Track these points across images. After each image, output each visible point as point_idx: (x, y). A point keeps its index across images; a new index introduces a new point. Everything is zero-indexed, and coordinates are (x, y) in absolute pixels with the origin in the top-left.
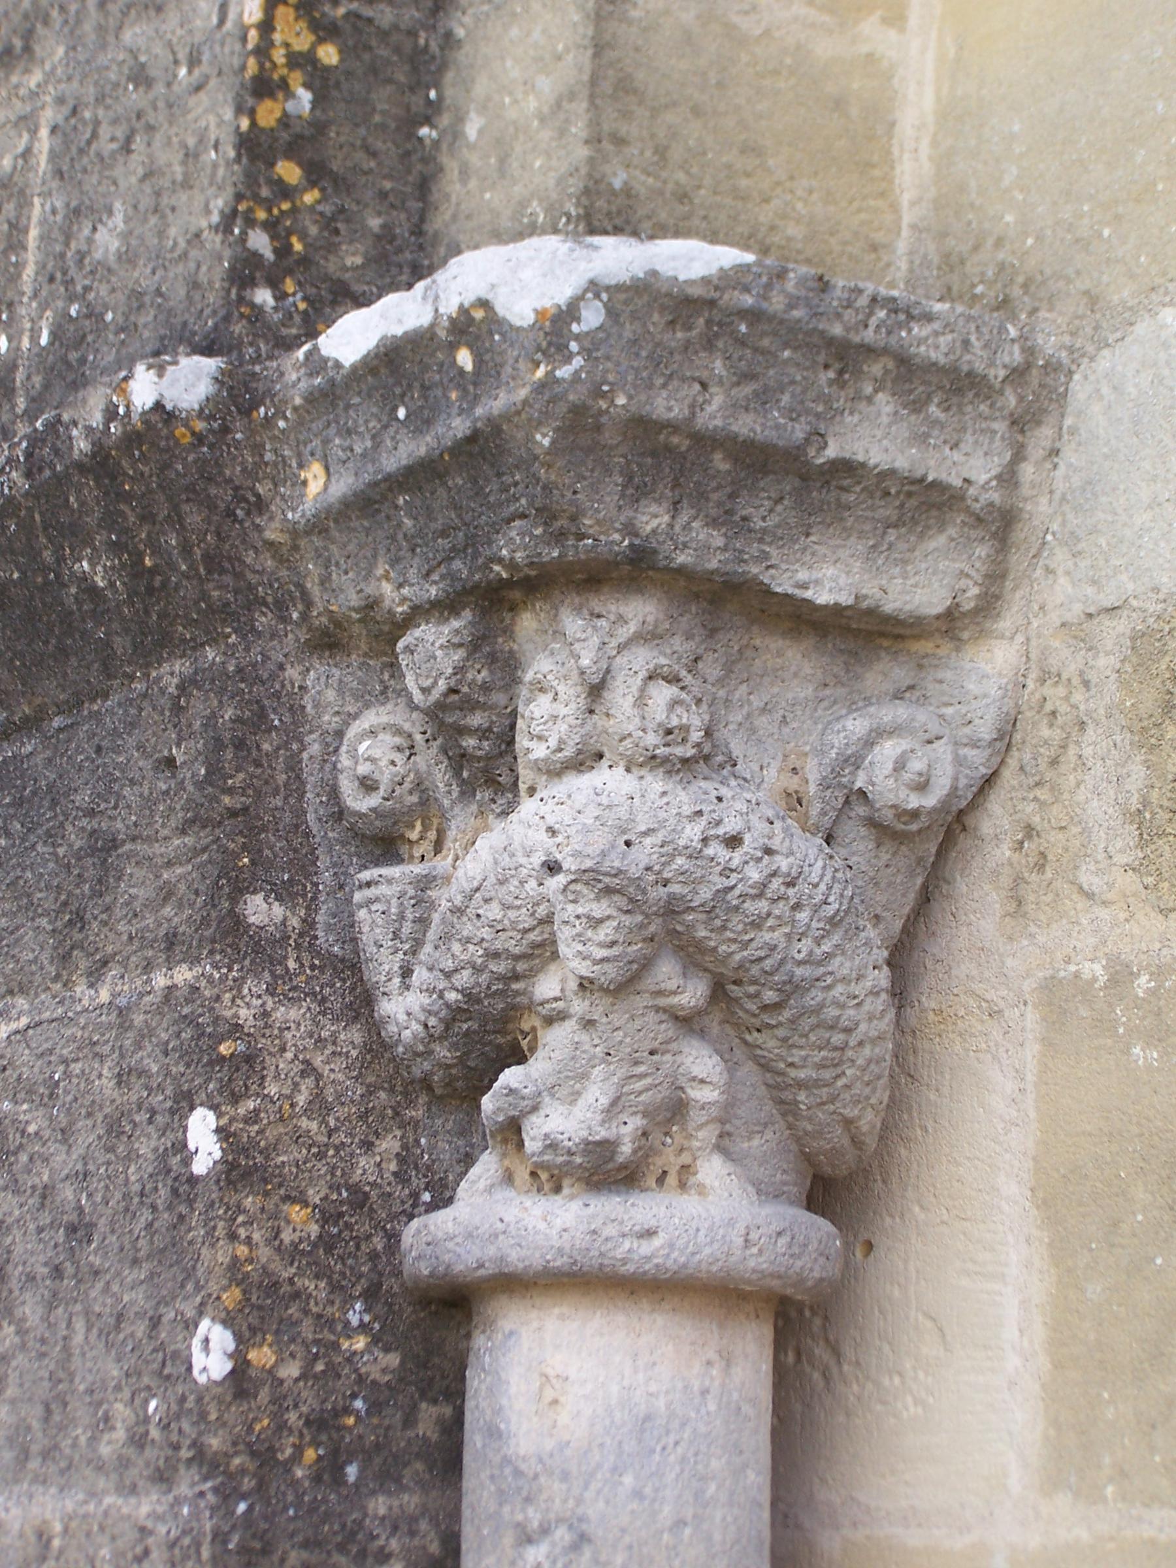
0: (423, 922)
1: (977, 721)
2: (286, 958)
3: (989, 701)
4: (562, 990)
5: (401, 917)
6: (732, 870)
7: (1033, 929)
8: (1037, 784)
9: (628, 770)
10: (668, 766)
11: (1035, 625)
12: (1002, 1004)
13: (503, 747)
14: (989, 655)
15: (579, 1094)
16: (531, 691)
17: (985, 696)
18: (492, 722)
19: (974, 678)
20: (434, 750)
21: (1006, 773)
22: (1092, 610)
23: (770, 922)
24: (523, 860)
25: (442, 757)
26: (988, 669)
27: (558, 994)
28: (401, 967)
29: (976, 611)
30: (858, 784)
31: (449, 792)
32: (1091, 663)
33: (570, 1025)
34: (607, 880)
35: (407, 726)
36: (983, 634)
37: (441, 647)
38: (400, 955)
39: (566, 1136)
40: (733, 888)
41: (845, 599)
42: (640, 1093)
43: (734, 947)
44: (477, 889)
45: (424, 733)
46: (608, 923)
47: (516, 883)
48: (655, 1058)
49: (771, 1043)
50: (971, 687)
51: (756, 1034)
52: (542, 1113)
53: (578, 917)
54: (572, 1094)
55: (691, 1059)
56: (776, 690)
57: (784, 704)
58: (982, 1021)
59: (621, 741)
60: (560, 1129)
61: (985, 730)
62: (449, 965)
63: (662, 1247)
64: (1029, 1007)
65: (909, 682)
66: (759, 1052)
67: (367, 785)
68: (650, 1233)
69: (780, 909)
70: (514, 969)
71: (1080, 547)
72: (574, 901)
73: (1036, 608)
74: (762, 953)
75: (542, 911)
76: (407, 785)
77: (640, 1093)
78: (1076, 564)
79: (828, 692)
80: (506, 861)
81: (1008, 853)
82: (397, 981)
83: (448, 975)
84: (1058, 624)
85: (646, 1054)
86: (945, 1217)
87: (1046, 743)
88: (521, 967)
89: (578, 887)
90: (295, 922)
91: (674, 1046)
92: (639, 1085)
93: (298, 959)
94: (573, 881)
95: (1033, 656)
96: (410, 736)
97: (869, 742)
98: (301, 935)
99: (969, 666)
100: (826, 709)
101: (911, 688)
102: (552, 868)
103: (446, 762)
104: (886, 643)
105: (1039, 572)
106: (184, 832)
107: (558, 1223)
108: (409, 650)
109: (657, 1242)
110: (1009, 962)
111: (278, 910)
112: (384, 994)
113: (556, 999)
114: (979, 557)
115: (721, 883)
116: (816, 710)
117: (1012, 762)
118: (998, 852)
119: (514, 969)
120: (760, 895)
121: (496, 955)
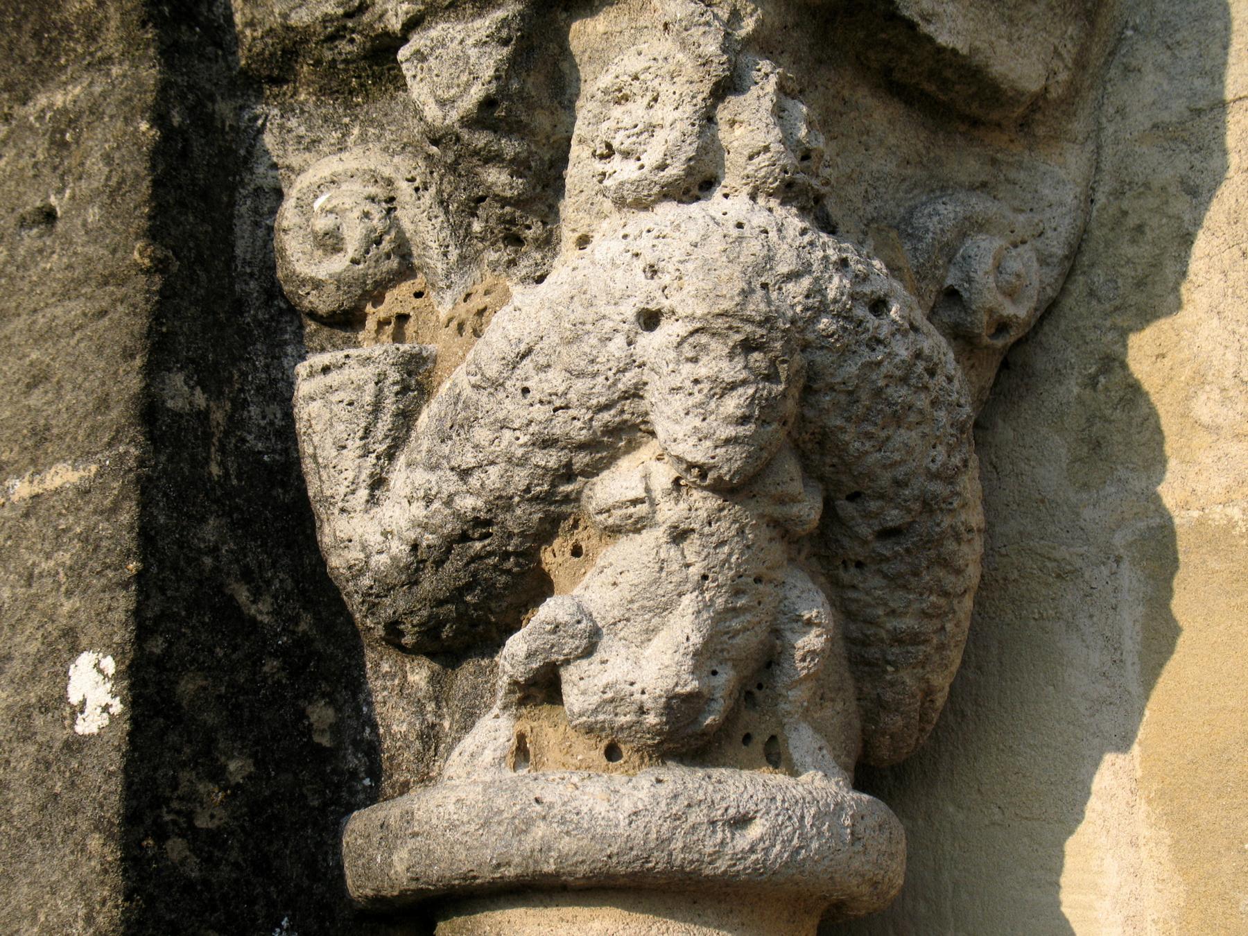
0: (406, 418)
1: (1049, 233)
2: (207, 460)
3: (1064, 210)
4: (648, 490)
5: (377, 408)
6: (879, 342)
7: (1121, 472)
8: (1117, 309)
9: (753, 197)
10: (803, 200)
11: (1111, 130)
12: (1079, 563)
13: (539, 189)
14: (1062, 160)
15: (655, 630)
16: (604, 103)
17: (1061, 204)
18: (530, 153)
19: (1049, 182)
20: (428, 197)
21: (1069, 302)
22: (1202, 104)
23: (913, 417)
24: (609, 310)
25: (438, 210)
26: (1062, 173)
27: (641, 493)
28: (372, 475)
29: (1062, 101)
30: (949, 281)
31: (445, 254)
32: (1198, 165)
33: (654, 537)
34: (749, 328)
35: (387, 172)
36: (1056, 137)
37: (481, 44)
38: (372, 459)
39: (637, 687)
40: (879, 364)
41: (962, 47)
42: (737, 633)
43: (868, 446)
44: (529, 352)
45: (412, 180)
46: (741, 390)
47: (594, 341)
48: (761, 587)
49: (877, 581)
50: (1047, 191)
51: (853, 570)
52: (597, 657)
53: (696, 382)
54: (647, 631)
55: (797, 592)
56: (859, 158)
57: (867, 177)
58: (1048, 585)
59: (751, 158)
60: (630, 678)
61: (1057, 247)
62: (469, 460)
63: (761, 839)
64: (1125, 565)
65: (983, 178)
66: (854, 595)
67: (330, 242)
68: (741, 822)
69: (922, 401)
70: (569, 465)
71: (1178, 37)
72: (694, 360)
73: (1111, 111)
74: (897, 457)
75: (628, 379)
76: (386, 246)
77: (737, 633)
78: (1174, 56)
79: (909, 171)
80: (579, 313)
81: (1076, 390)
82: (363, 493)
83: (464, 474)
84: (1148, 125)
85: (750, 580)
86: (998, 817)
87: (1128, 261)
88: (581, 460)
89: (704, 339)
90: (218, 416)
91: (779, 575)
92: (736, 624)
93: (221, 464)
94: (697, 331)
95: (1106, 166)
96: (390, 182)
97: (972, 226)
98: (227, 434)
99: (1043, 168)
100: (907, 192)
101: (984, 185)
102: (650, 319)
103: (442, 218)
104: (962, 128)
105: (1114, 72)
106: (65, 296)
107: (628, 806)
108: (420, 56)
109: (755, 830)
110: (1087, 513)
111: (200, 399)
112: (343, 510)
113: (635, 502)
114: (1072, 38)
115: (866, 355)
116: (897, 191)
117: (1079, 285)
118: (1062, 390)
119: (569, 465)
120: (904, 380)
121: (547, 443)
